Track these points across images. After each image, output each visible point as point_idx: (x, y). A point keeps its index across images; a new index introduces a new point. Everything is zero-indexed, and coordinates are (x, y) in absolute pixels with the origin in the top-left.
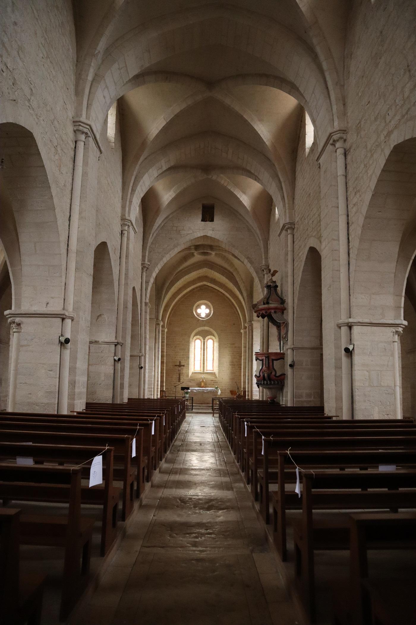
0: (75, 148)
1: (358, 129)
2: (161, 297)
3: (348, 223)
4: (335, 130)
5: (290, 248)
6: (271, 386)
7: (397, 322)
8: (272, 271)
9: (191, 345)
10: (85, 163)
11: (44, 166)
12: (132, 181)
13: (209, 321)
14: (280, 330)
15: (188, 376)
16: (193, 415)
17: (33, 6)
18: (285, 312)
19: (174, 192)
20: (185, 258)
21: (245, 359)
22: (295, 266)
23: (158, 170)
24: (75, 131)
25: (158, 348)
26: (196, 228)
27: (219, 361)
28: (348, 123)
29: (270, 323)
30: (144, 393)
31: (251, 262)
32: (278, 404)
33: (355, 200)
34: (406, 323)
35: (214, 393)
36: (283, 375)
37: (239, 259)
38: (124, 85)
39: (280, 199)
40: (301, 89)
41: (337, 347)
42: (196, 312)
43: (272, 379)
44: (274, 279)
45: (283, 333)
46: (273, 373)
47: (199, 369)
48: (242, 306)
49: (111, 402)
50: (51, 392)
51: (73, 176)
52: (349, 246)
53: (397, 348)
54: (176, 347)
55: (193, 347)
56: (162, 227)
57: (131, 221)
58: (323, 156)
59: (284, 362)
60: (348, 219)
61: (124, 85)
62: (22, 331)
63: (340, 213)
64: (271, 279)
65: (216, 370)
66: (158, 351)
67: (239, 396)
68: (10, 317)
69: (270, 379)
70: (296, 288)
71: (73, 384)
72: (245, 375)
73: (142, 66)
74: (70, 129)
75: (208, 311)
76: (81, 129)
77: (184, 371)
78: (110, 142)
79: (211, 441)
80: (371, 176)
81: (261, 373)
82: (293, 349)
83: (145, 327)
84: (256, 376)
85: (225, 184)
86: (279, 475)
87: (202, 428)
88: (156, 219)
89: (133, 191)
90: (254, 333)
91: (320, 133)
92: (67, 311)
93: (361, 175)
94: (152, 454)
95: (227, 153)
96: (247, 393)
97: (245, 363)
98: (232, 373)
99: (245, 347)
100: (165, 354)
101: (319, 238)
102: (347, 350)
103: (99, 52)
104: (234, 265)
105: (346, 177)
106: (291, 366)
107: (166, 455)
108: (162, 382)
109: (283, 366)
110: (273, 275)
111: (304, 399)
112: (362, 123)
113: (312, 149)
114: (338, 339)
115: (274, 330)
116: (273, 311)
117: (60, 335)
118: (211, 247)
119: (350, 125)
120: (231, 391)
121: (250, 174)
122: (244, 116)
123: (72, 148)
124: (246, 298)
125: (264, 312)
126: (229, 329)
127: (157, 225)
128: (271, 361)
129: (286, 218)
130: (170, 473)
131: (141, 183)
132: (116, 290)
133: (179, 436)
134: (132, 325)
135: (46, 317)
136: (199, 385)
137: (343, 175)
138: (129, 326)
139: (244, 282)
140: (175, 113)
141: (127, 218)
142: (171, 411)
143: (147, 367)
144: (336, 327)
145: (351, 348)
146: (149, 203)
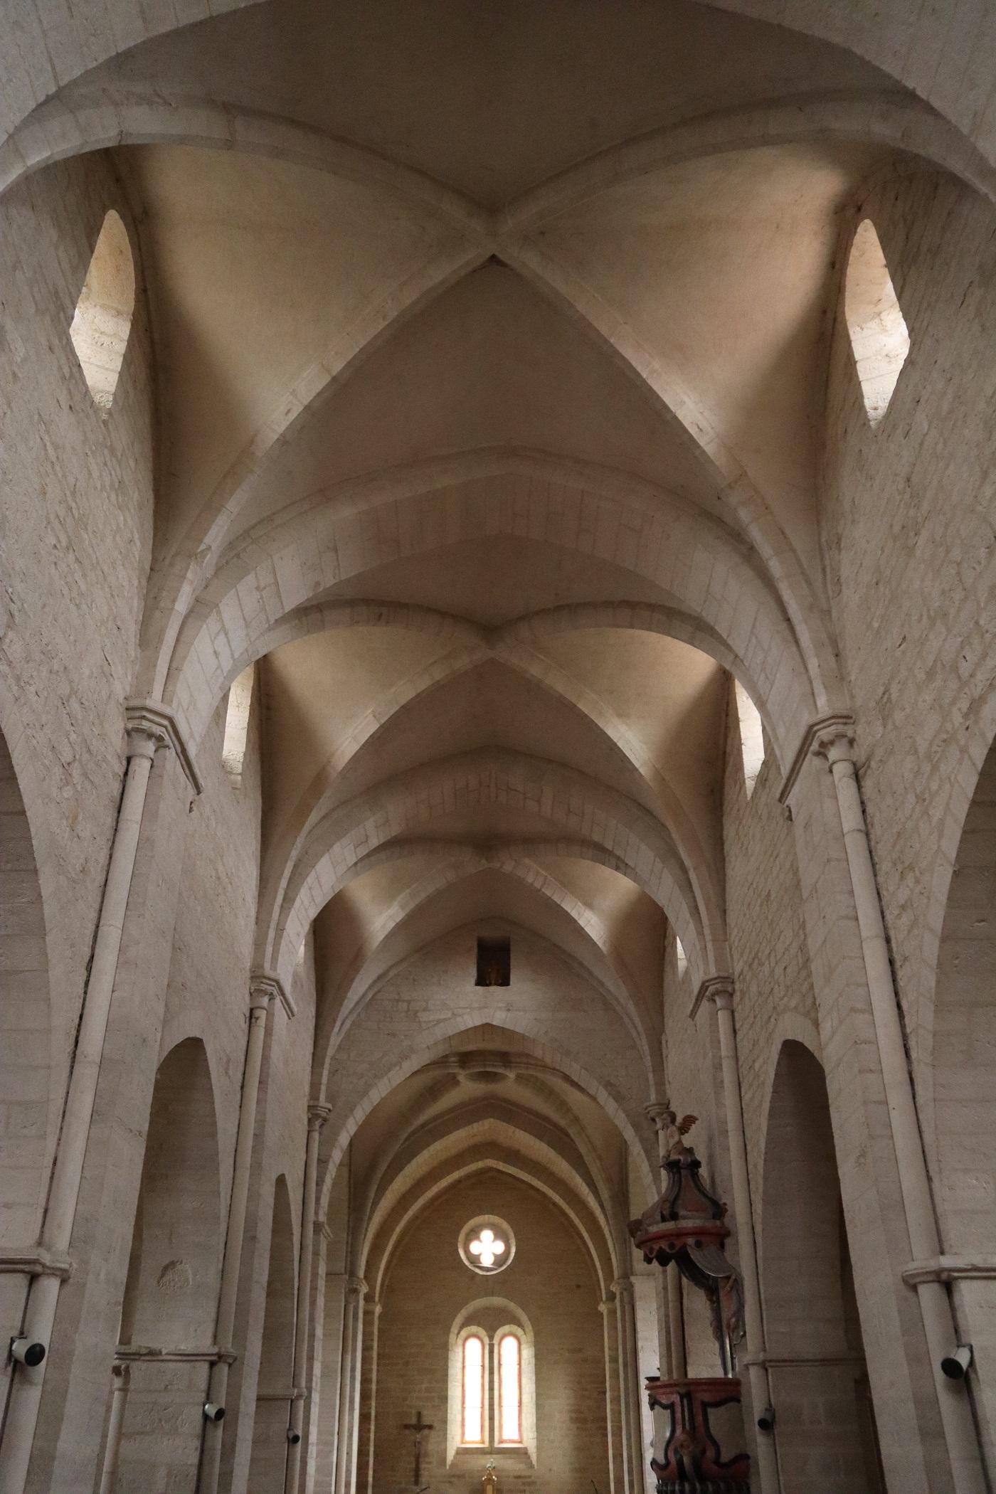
0: (126, 774)
1: (885, 708)
3: (891, 962)
4: (821, 716)
5: (725, 1050)
8: (679, 1119)
9: (451, 1355)
11: (23, 813)
12: (287, 874)
13: (504, 1278)
14: (718, 1301)
17: (46, 438)
18: (728, 1241)
19: (402, 907)
21: (616, 1400)
22: (746, 1098)
24: (128, 733)
25: (353, 1369)
26: (462, 1005)
27: (539, 1406)
28: (852, 697)
29: (685, 1280)
31: (618, 1097)
33: (903, 895)
36: (743, 1460)
38: (269, 629)
40: (722, 629)
41: (917, 1357)
42: (467, 1251)
44: (688, 1140)
45: (727, 1311)
46: (710, 1454)
47: (478, 1438)
48: (599, 1228)
51: (112, 848)
52: (903, 1026)
54: (407, 1363)
55: (459, 1365)
56: (370, 1003)
57: (277, 982)
60: (890, 950)
61: (269, 629)
63: (864, 933)
64: (680, 1142)
65: (530, 1441)
70: (755, 1166)
72: (618, 1456)
73: (318, 584)
74: (116, 726)
75: (499, 1247)
76: (147, 728)
78: (231, 773)
80: (942, 822)
81: (671, 1454)
82: (764, 1366)
83: (313, 1303)
84: (654, 1463)
85: (537, 885)
88: (352, 981)
89: (289, 900)
90: (640, 1314)
91: (781, 731)
92: (49, 1249)
93: (909, 825)
95: (539, 801)
97: (617, 1413)
99: (614, 1360)
100: (374, 1387)
101: (812, 1014)
102: (951, 1367)
103: (209, 548)
104: (569, 1110)
105: (867, 834)
106: (766, 1425)
109: (738, 1426)
110: (684, 1129)
112: (894, 689)
113: (762, 778)
114: (913, 1326)
115: (697, 1302)
117: (15, 1333)
118: (505, 1058)
119: (859, 702)
121: (603, 854)
122: (580, 706)
123: (115, 774)
124: (608, 1205)
125: (664, 1245)
126: (566, 1313)
127: (356, 998)
128: (698, 1410)
129: (707, 964)
131: (310, 879)
137: (860, 830)
138: (259, 1297)
139: (600, 1158)
140: (403, 702)
141: (267, 970)
143: (313, 1438)
144: (902, 1286)
145: (963, 1358)
146: (333, 934)
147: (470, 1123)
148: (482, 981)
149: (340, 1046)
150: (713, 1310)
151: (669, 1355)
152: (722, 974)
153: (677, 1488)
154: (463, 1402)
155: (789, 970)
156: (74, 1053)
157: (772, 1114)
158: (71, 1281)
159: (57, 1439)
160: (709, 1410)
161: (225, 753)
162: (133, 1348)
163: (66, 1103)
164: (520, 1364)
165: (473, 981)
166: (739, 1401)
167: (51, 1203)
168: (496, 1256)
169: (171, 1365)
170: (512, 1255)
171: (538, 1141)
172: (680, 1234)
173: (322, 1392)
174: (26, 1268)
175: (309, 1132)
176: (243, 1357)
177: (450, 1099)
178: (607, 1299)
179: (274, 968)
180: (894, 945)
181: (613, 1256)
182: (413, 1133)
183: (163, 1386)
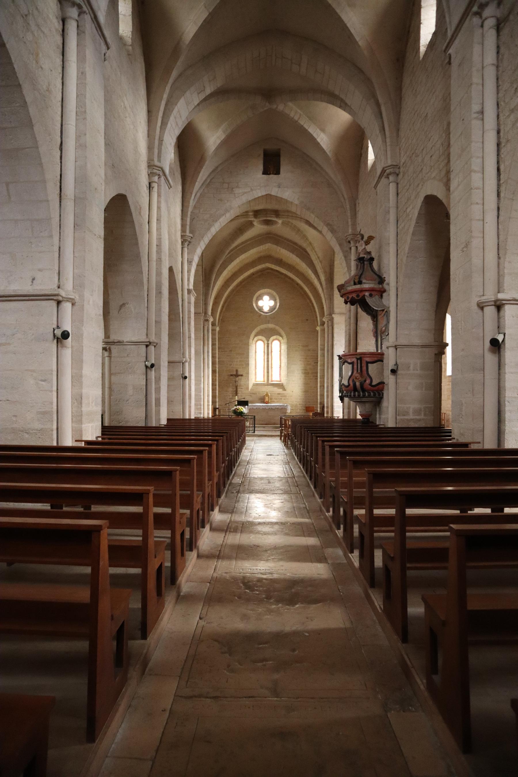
2: (210, 283)
6: (364, 400)
9: (250, 348)
10: (159, 196)
13: (274, 316)
15: (248, 388)
16: (255, 438)
19: (224, 132)
22: (400, 227)
23: (198, 94)
25: (208, 352)
26: (254, 186)
31: (333, 231)
35: (283, 409)
37: (315, 228)
39: (378, 132)
43: (364, 390)
44: (369, 248)
46: (368, 381)
47: (262, 380)
49: (144, 425)
50: (44, 413)
54: (231, 351)
55: (254, 351)
57: (162, 168)
58: (457, 42)
59: (383, 365)
60: (499, 138)
66: (208, 356)
67: (316, 414)
69: (363, 390)
70: (402, 260)
71: (78, 399)
75: (272, 303)
77: (242, 381)
82: (396, 347)
83: (189, 324)
85: (296, 118)
87: (266, 457)
89: (164, 124)
90: (336, 330)
94: (208, 490)
95: (299, 65)
96: (325, 410)
99: (323, 349)
100: (217, 360)
104: (307, 239)
106: (394, 372)
107: (220, 501)
108: (214, 397)
109: (381, 372)
110: (367, 243)
111: (411, 417)
115: (366, 323)
116: (367, 294)
117: (55, 326)
118: (277, 213)
120: (306, 407)
123: (57, 30)
124: (324, 283)
125: (354, 295)
126: (303, 323)
128: (364, 365)
130: (226, 532)
132: (145, 269)
133: (239, 470)
134: (170, 320)
139: (321, 262)
141: (156, 163)
143: (193, 377)
145: (500, 338)
146: (188, 144)
148: (265, 172)
149: (195, 206)
150: (373, 324)
151: (349, 345)
152: (395, 164)
153: (352, 394)
154: (256, 366)
156: (60, 194)
157: (413, 234)
158: (76, 304)
160: (369, 364)
161: (121, 31)
162: (111, 340)
163: (60, 220)
164: (280, 351)
165: (261, 172)
166: (382, 361)
167: (61, 269)
168: (270, 307)
169: (129, 347)
170: (278, 306)
171: (291, 254)
172: (362, 291)
173: (195, 361)
174: (55, 298)
175: (182, 248)
176: (160, 343)
178: (321, 325)
179: (159, 161)
180: (502, 134)
181: (325, 306)
182: (232, 250)
183: (126, 355)
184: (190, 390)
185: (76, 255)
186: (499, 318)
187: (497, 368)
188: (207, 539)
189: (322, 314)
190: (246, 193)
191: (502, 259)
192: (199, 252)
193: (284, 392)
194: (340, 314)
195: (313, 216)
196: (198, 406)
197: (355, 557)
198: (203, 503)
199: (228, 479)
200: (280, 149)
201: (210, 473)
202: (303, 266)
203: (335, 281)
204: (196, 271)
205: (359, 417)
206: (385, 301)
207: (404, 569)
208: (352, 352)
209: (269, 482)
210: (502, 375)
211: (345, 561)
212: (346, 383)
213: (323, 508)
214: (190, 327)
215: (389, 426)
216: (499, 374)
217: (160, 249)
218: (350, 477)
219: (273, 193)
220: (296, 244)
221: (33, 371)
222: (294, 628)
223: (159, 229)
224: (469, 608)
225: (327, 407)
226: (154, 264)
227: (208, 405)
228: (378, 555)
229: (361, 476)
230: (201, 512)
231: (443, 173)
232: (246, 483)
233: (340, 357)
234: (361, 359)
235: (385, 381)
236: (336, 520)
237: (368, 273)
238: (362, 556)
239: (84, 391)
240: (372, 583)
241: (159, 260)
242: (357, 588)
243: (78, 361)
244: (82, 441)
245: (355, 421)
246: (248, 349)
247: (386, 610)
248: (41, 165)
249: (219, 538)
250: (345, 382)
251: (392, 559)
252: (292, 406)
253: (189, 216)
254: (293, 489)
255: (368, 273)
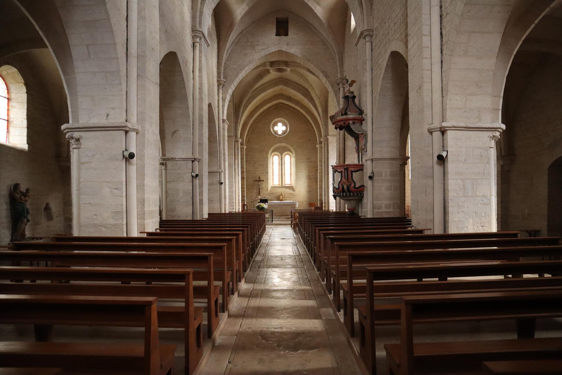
6: (350, 198)
7: (496, 125)
8: (349, 82)
10: (200, 52)
13: (285, 137)
16: (273, 226)
18: (363, 122)
19: (248, 5)
20: (260, 76)
22: (374, 74)
25: (238, 164)
26: (270, 44)
30: (225, 208)
31: (327, 76)
32: (357, 215)
34: (504, 127)
35: (293, 205)
37: (314, 74)
39: (357, 6)
43: (350, 191)
44: (352, 89)
50: (117, 212)
53: (493, 153)
54: (255, 163)
60: (441, 11)
62: (82, 147)
64: (349, 89)
66: (238, 167)
67: (317, 208)
68: (68, 132)
69: (349, 191)
70: (375, 97)
71: (142, 202)
75: (284, 128)
77: (263, 185)
79: (291, 254)
81: (340, 185)
82: (372, 160)
83: (224, 144)
86: (348, 273)
87: (281, 241)
90: (330, 147)
94: (236, 268)
98: (309, 186)
99: (321, 161)
104: (309, 82)
106: (371, 178)
107: (246, 275)
108: (243, 196)
109: (362, 177)
110: (351, 85)
111: (384, 210)
115: (351, 142)
116: (351, 122)
117: (124, 149)
118: (286, 63)
124: (321, 114)
125: (342, 123)
126: (306, 143)
133: (261, 250)
134: (210, 141)
135: (106, 130)
136: (278, 198)
139: (319, 98)
141: (198, 28)
142: (248, 227)
144: (427, 132)
145: (444, 154)
147: (274, 87)
148: (278, 34)
152: (369, 28)
155: (396, 24)
159: (144, 180)
173: (229, 171)
174: (124, 129)
177: (267, 79)
179: (200, 27)
180: (443, 9)
184: (225, 192)
185: (139, 97)
186: (443, 140)
187: (443, 176)
188: (236, 303)
189: (320, 136)
190: (264, 49)
191: (445, 97)
192: (230, 92)
193: (294, 192)
194: (333, 135)
195: (312, 65)
196: (231, 204)
197: (341, 315)
198: (232, 276)
199: (252, 257)
200: (287, 18)
201: (238, 255)
202: (306, 102)
203: (329, 112)
204: (229, 106)
205: (347, 210)
206: (363, 127)
207: (373, 325)
208: (341, 164)
209: (282, 260)
210: (446, 181)
211: (334, 318)
212: (337, 186)
213: (320, 279)
214: (225, 146)
215: (368, 217)
216: (444, 180)
217: (202, 91)
218: (337, 257)
219: (283, 50)
220: (300, 85)
221: (108, 182)
222: (296, 368)
223: (200, 77)
224: (415, 355)
225: (325, 203)
226: (197, 102)
227: (239, 203)
228: (356, 312)
229: (345, 256)
230: (231, 283)
231: (403, 35)
232: (265, 260)
233: (334, 167)
234: (347, 169)
235: (365, 184)
236: (329, 288)
237: (352, 107)
238: (345, 314)
239: (146, 196)
240: (353, 334)
241: (201, 99)
242: (342, 338)
243: (141, 175)
244: (145, 233)
245: (344, 213)
246: (267, 162)
247: (361, 354)
248: (112, 32)
249: (244, 302)
250: (337, 186)
251: (365, 318)
252: (299, 202)
253: (223, 66)
254: (299, 264)
255: (352, 107)
